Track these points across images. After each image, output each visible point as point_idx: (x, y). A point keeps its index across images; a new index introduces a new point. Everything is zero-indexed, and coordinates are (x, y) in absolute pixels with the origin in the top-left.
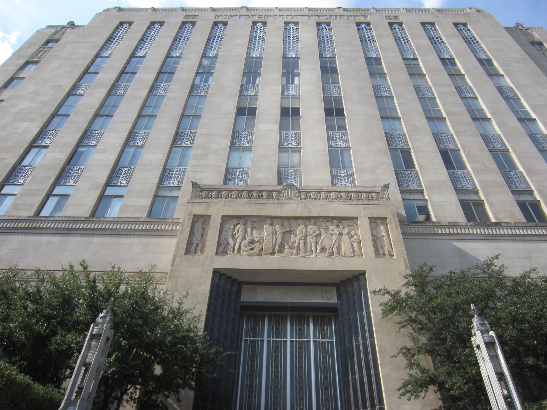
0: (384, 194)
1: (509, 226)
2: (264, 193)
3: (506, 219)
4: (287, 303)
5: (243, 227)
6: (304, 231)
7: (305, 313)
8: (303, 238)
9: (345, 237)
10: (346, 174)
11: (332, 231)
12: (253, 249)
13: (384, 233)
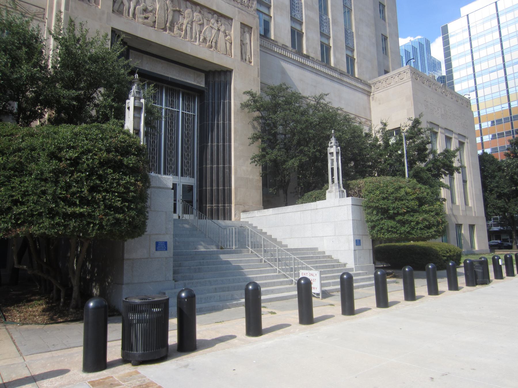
1: (313, 60)
3: (281, 42)
6: (191, 16)
8: (190, 23)
9: (221, 34)
11: (213, 24)
12: (146, 18)
13: (248, 41)
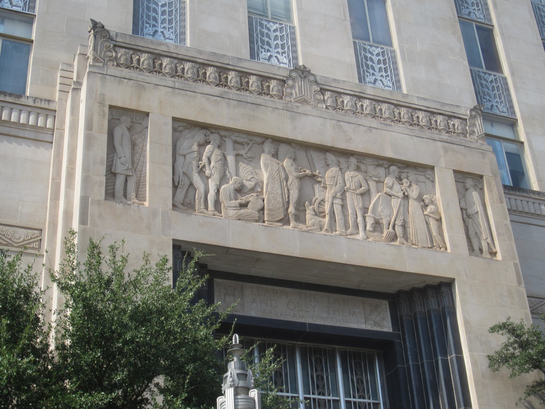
0: (474, 125)
2: (252, 79)
4: (305, 324)
5: (217, 152)
7: (327, 346)
8: (338, 195)
9: (413, 205)
10: (381, 58)
11: (391, 188)
13: (478, 207)
